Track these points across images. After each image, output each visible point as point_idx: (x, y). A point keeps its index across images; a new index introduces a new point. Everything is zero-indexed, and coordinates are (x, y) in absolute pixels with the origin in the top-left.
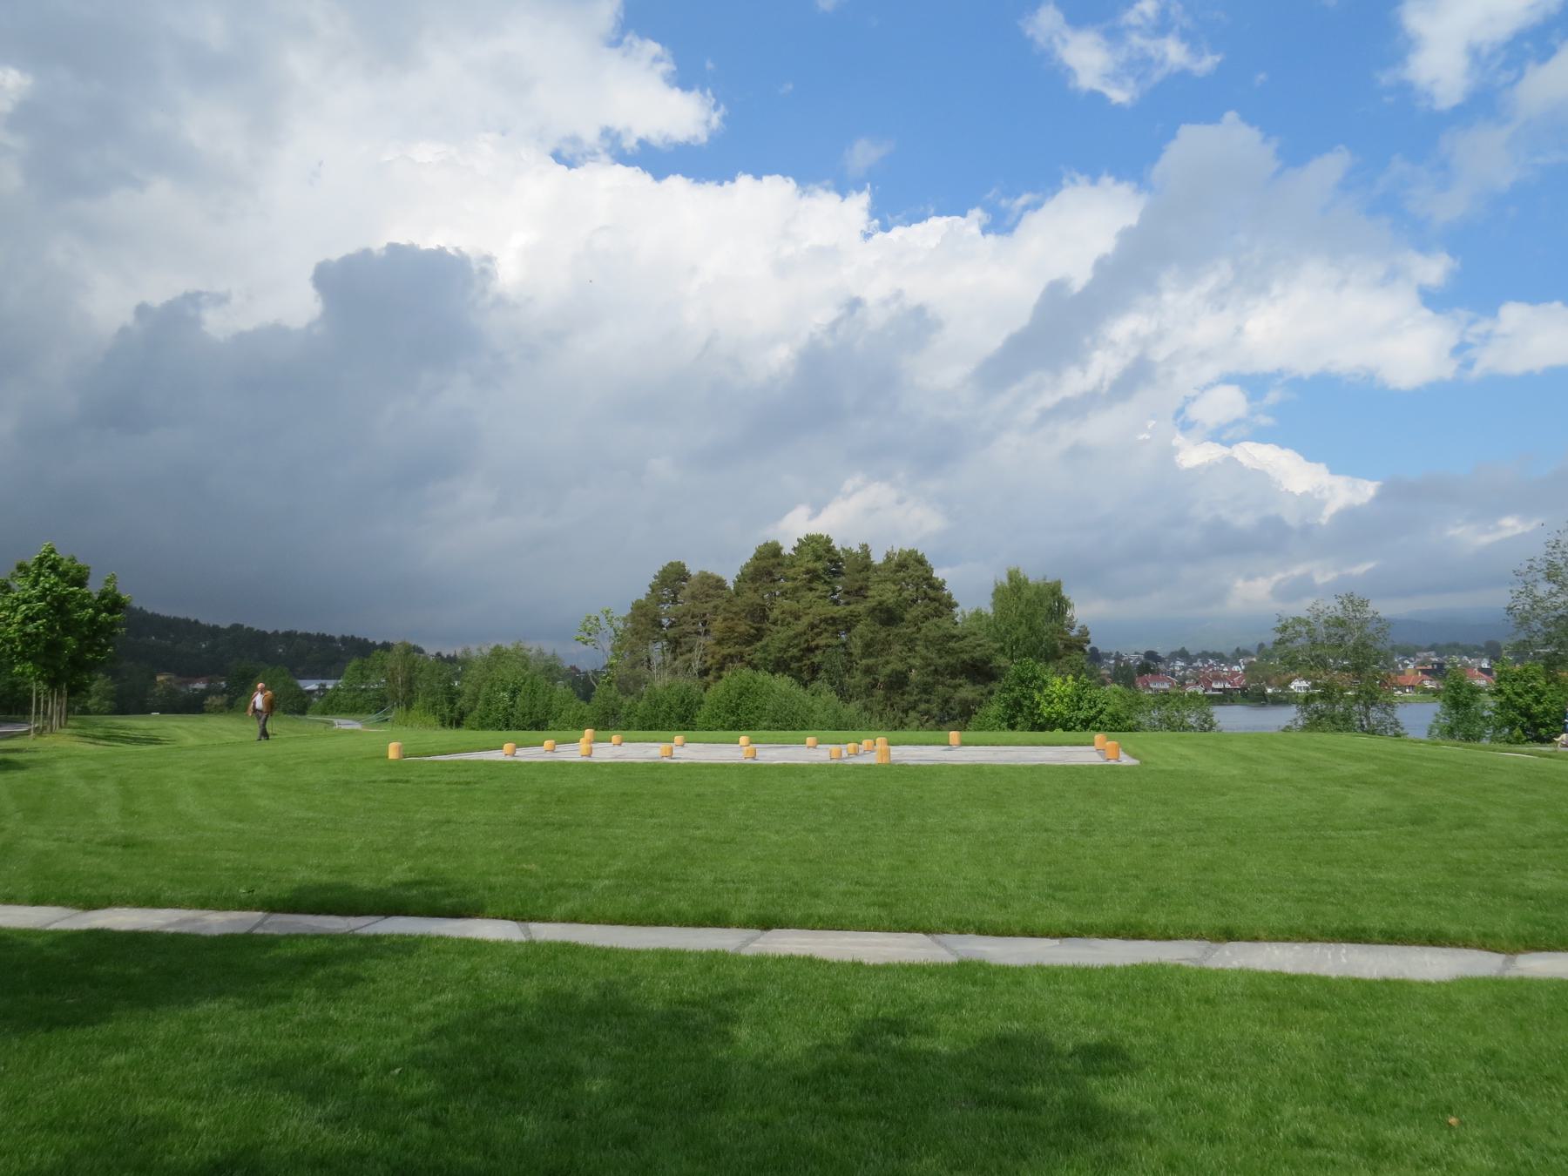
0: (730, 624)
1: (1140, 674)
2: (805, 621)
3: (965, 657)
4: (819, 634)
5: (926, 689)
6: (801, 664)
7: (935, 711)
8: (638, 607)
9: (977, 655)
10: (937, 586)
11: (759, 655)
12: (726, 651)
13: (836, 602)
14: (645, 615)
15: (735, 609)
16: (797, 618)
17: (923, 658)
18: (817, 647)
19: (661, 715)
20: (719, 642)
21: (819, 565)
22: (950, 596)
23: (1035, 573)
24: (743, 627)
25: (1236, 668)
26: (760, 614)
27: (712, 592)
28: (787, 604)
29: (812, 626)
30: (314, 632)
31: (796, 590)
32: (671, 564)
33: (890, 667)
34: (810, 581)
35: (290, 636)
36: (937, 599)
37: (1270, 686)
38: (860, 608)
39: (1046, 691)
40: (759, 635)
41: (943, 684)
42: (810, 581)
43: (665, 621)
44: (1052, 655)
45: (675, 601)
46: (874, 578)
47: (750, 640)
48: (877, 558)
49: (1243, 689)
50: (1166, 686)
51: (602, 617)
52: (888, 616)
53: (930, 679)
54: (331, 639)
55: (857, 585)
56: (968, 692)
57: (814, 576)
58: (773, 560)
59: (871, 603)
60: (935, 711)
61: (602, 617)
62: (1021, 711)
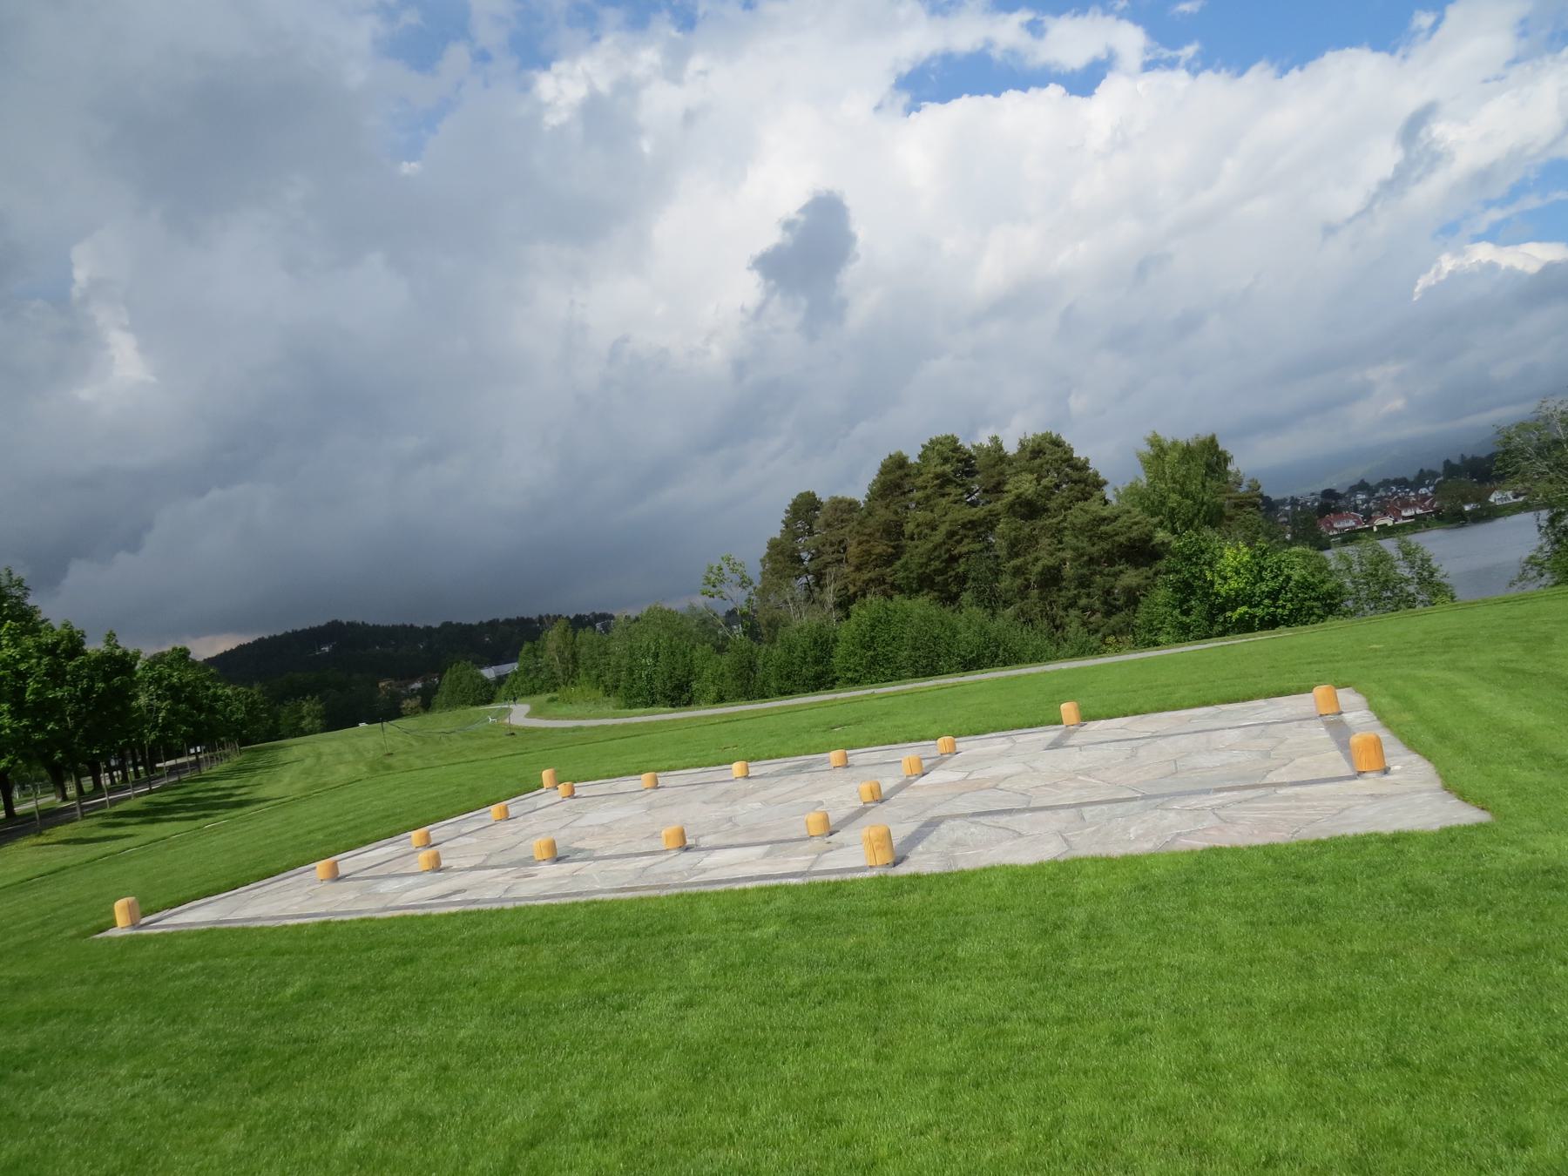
0: (865, 547)
1: (1322, 517)
2: (943, 529)
3: (1122, 539)
4: (959, 542)
5: (1084, 583)
6: (942, 582)
7: (1097, 605)
8: (774, 545)
9: (1134, 535)
10: (1082, 467)
11: (901, 574)
12: (866, 576)
13: (973, 504)
14: (782, 553)
15: (867, 531)
16: (934, 528)
17: (1075, 549)
18: (961, 556)
19: (797, 661)
20: (858, 568)
21: (948, 468)
22: (1096, 475)
23: (1182, 429)
24: (881, 548)
25: (1423, 491)
26: (894, 531)
27: (845, 516)
28: (921, 515)
29: (951, 534)
30: (514, 617)
31: (928, 498)
32: (801, 496)
33: (1040, 564)
34: (941, 486)
35: (493, 624)
36: (1084, 482)
37: (1467, 503)
38: (998, 506)
39: (1218, 566)
40: (898, 552)
41: (1101, 573)
42: (941, 486)
43: (804, 555)
44: (1216, 518)
45: (811, 533)
46: (1009, 471)
47: (889, 560)
48: (1011, 448)
49: (1437, 511)
50: (1352, 523)
51: (724, 566)
52: (1030, 509)
53: (1085, 571)
54: (530, 621)
55: (994, 481)
56: (1131, 577)
57: (944, 481)
58: (899, 473)
59: (1008, 498)
60: (1097, 605)
61: (724, 566)
62: (1194, 593)
